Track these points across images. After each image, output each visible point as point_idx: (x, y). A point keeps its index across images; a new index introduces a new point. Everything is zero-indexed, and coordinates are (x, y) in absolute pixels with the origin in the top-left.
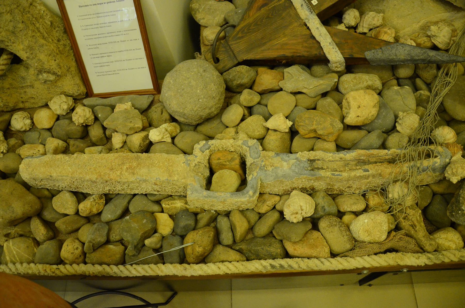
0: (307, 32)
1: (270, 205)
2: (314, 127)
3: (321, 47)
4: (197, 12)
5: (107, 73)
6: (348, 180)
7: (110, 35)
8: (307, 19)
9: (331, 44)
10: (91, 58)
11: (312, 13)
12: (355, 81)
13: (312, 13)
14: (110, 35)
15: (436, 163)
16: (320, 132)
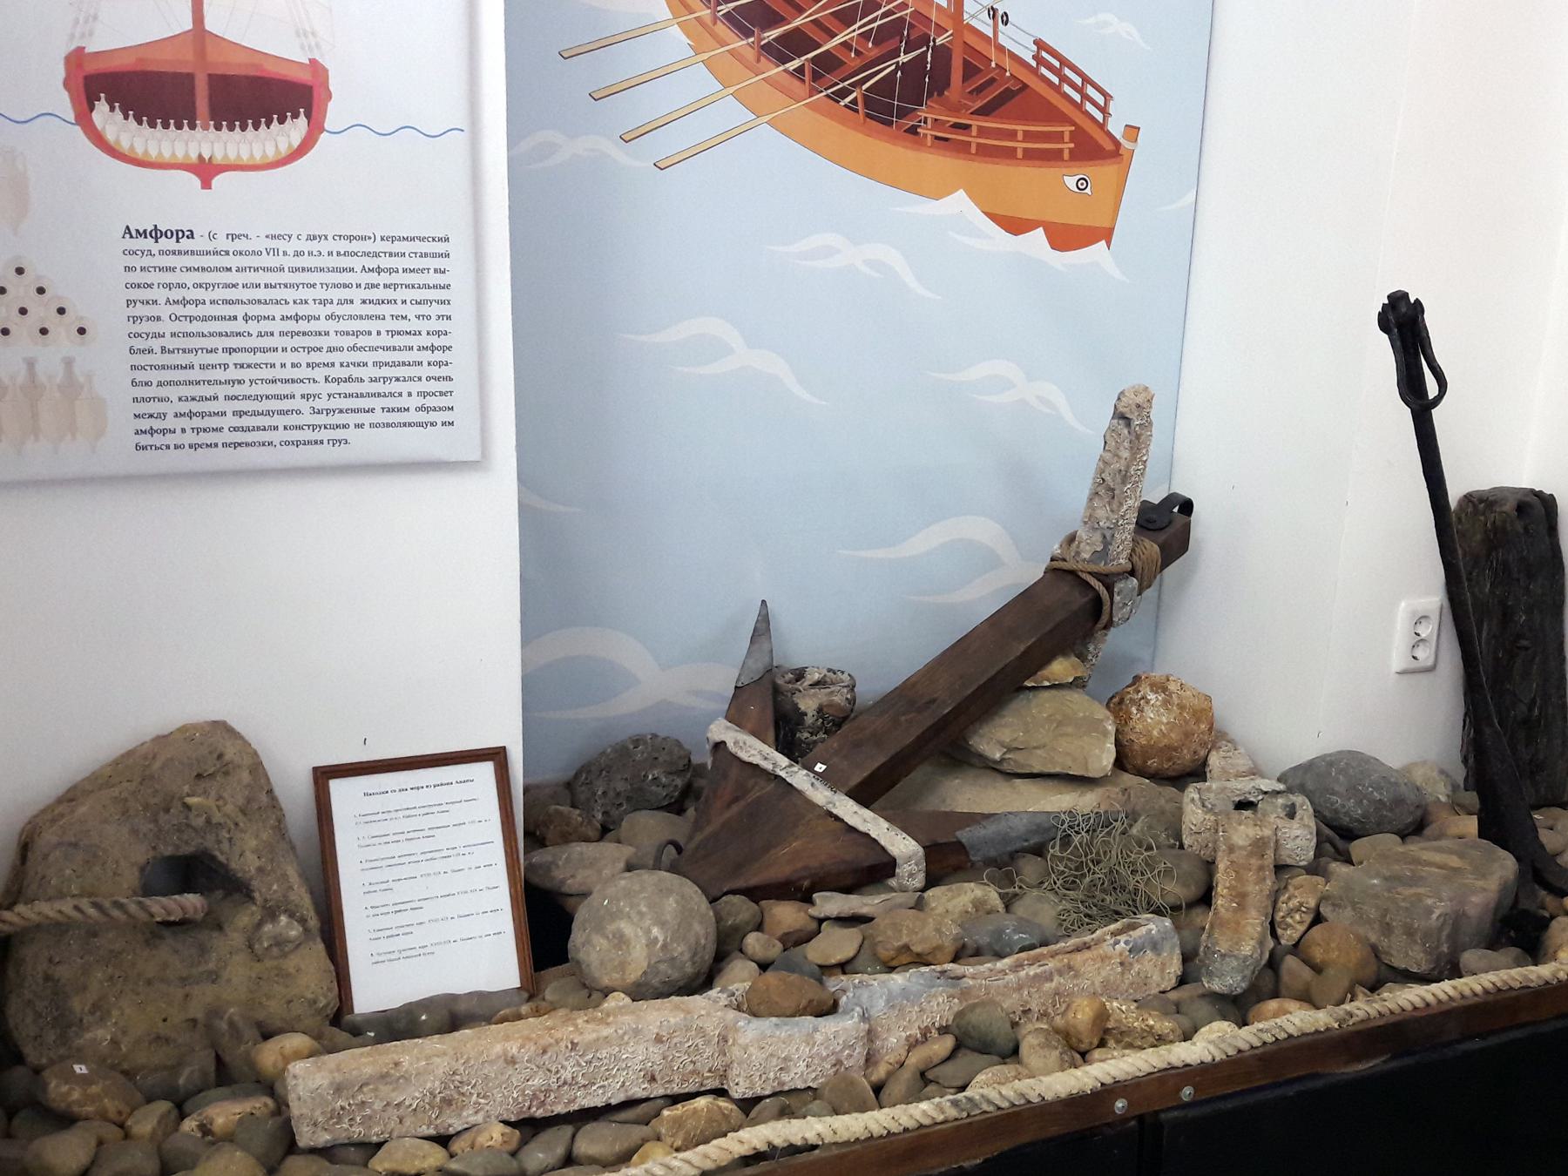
1: (891, 1061)
2: (905, 940)
3: (875, 840)
4: (553, 867)
5: (405, 954)
6: (1019, 988)
7: (429, 856)
8: (830, 803)
10: (368, 916)
11: (835, 792)
12: (950, 894)
13: (835, 792)
14: (429, 856)
15: (1151, 930)
16: (917, 948)
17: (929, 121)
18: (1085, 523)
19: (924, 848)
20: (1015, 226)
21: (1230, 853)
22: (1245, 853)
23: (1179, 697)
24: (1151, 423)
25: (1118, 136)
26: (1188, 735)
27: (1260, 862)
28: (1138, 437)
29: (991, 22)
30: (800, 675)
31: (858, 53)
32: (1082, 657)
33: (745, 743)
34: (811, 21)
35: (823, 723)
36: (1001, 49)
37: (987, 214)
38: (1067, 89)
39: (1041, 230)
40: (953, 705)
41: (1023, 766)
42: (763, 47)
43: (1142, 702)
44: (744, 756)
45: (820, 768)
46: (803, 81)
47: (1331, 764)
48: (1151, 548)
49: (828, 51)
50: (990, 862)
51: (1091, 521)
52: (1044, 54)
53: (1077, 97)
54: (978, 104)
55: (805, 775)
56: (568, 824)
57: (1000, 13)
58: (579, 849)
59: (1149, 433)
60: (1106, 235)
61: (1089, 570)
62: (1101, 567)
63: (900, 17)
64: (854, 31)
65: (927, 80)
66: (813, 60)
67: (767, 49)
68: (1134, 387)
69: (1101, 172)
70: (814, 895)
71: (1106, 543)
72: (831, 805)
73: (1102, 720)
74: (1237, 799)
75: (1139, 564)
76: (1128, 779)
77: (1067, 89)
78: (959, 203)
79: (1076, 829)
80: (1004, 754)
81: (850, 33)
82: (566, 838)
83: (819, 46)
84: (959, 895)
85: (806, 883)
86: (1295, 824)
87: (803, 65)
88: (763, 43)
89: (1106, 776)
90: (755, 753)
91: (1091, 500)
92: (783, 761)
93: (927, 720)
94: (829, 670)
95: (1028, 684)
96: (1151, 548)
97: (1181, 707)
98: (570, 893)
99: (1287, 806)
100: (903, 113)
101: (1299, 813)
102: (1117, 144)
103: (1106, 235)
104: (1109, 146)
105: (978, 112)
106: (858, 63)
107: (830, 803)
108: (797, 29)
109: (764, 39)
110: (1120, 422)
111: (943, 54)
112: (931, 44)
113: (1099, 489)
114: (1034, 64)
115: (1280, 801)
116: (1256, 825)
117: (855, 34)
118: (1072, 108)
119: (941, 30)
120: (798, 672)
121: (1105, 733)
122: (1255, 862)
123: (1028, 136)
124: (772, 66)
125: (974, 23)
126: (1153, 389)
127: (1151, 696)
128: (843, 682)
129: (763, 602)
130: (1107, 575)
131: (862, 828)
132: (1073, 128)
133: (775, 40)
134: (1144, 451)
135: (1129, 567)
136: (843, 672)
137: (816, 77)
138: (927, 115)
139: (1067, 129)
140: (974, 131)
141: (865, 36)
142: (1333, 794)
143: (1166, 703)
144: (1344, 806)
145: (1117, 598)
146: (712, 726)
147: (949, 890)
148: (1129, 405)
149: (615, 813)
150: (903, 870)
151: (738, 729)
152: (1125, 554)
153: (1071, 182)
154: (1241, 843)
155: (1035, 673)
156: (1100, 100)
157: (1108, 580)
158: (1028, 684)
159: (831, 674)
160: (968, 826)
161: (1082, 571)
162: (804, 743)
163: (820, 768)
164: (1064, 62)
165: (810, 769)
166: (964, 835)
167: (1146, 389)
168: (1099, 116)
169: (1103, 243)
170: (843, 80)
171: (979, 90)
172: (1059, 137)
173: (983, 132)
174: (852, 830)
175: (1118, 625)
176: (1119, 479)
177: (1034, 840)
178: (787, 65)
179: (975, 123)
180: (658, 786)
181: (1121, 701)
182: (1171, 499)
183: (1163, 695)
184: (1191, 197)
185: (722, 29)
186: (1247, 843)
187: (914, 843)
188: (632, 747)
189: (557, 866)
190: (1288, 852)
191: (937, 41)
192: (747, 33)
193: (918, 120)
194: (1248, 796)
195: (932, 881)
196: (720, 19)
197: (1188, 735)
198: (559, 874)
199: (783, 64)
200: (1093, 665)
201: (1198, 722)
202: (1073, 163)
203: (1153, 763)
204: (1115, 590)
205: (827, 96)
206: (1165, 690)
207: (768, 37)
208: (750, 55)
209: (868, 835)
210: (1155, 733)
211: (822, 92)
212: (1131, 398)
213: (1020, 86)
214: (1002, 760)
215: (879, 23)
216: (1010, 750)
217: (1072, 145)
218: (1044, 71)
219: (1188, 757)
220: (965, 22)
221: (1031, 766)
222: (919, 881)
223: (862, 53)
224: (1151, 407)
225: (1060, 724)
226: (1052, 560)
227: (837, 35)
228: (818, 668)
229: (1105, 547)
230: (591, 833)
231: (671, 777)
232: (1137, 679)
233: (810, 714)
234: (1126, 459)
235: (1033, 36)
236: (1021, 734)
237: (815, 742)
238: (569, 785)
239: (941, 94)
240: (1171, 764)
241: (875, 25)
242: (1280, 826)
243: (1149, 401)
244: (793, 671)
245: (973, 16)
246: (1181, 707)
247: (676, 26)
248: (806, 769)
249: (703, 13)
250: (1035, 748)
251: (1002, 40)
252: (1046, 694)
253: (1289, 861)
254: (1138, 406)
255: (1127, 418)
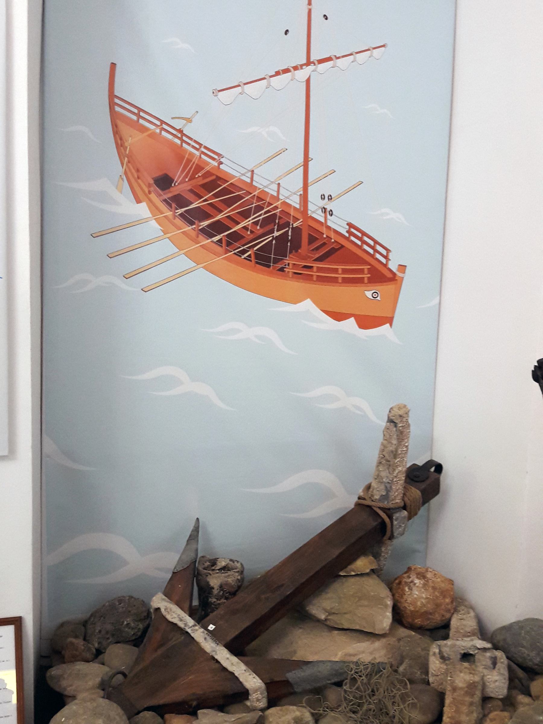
0: (217, 665)
9: (246, 671)
11: (218, 644)
12: (281, 713)
17: (290, 264)
18: (376, 479)
19: (265, 683)
20: (338, 316)
21: (453, 692)
22: (462, 692)
23: (433, 582)
24: (409, 426)
25: (394, 270)
26: (438, 605)
27: (471, 700)
28: (402, 433)
29: (323, 215)
30: (214, 562)
31: (252, 232)
32: (377, 556)
33: (171, 610)
34: (226, 217)
35: (223, 593)
36: (329, 228)
37: (322, 310)
38: (365, 247)
39: (352, 319)
40: (294, 588)
41: (337, 624)
42: (201, 230)
43: (411, 584)
44: (169, 617)
45: (211, 627)
46: (222, 246)
47: (522, 628)
48: (415, 493)
49: (235, 231)
50: (306, 692)
51: (378, 477)
52: (352, 230)
53: (371, 251)
54: (317, 256)
55: (201, 632)
56: (76, 650)
57: (328, 210)
58: (81, 666)
59: (408, 431)
60: (390, 320)
61: (378, 506)
62: (385, 504)
63: (274, 213)
64: (249, 221)
65: (289, 244)
66: (227, 236)
67: (203, 231)
68: (398, 405)
69: (387, 288)
70: (199, 711)
71: (388, 490)
72: (214, 653)
73: (383, 598)
74: (463, 652)
75: (408, 502)
76: (403, 632)
77: (365, 247)
78: (308, 305)
79: (360, 674)
80: (327, 616)
81: (246, 223)
82: (75, 659)
83: (231, 229)
84: (287, 714)
85: (194, 703)
86: (495, 673)
87: (221, 238)
88: (200, 228)
89: (385, 634)
90: (175, 616)
91: (378, 466)
92: (191, 622)
93: (277, 597)
94: (231, 560)
95: (342, 573)
96: (415, 493)
97: (434, 588)
98: (70, 695)
99: (492, 657)
100: (276, 261)
101: (499, 665)
102: (394, 274)
103: (390, 320)
104: (389, 275)
105: (316, 260)
106: (252, 236)
107: (214, 651)
108: (218, 221)
109: (201, 226)
110: (392, 424)
111: (297, 231)
112: (291, 226)
113: (382, 460)
114: (347, 235)
115: (488, 654)
116: (471, 673)
117: (250, 222)
118: (369, 257)
119: (296, 219)
120: (212, 561)
121: (386, 606)
122: (468, 699)
123: (345, 271)
124: (205, 239)
125: (314, 215)
126: (409, 407)
127: (417, 581)
128: (236, 569)
129: (198, 519)
130: (389, 509)
131: (230, 669)
132: (369, 267)
133: (207, 226)
134: (406, 440)
135: (402, 504)
136: (238, 562)
137: (229, 244)
138: (289, 262)
139: (366, 267)
140: (315, 269)
141: (256, 223)
142: (522, 647)
143: (425, 585)
144: (528, 655)
145: (395, 523)
146: (154, 598)
147: (281, 710)
148: (395, 415)
149: (105, 643)
150: (253, 696)
151: (169, 600)
152: (399, 497)
153: (369, 294)
154: (461, 685)
155: (346, 567)
156: (384, 252)
157: (390, 512)
158: (342, 573)
159: (231, 563)
160: (294, 670)
161: (374, 506)
162: (214, 605)
163: (211, 627)
164: (364, 234)
165: (206, 628)
166: (291, 676)
167: (405, 406)
168: (384, 260)
169: (388, 325)
170: (243, 246)
171: (317, 249)
172: (361, 271)
173: (319, 269)
174: (225, 669)
175: (397, 537)
176: (392, 456)
177: (336, 680)
178: (213, 239)
179: (316, 265)
180: (129, 628)
181: (400, 583)
182: (430, 463)
183: (424, 581)
184: (437, 301)
185: (179, 222)
186: (464, 685)
187: (260, 681)
188: (118, 604)
189: (64, 678)
190: (491, 690)
191: (294, 225)
192: (192, 223)
193: (285, 264)
194: (469, 650)
195: (272, 702)
196: (177, 217)
197: (438, 605)
198: (64, 683)
199: (211, 238)
200: (386, 558)
201: (444, 597)
202: (369, 284)
203: (418, 621)
204: (394, 518)
205: (235, 253)
206: (424, 577)
207: (203, 225)
208: (193, 234)
209: (233, 674)
210: (419, 604)
211: (231, 251)
212: (396, 412)
213: (340, 246)
214: (326, 620)
215: (263, 217)
216: (330, 614)
217: (369, 275)
218: (353, 238)
219: (439, 619)
220: (309, 215)
221: (342, 624)
222: (263, 704)
223: (254, 232)
224: (408, 417)
225: (360, 599)
226: (359, 498)
227: (240, 223)
228: (224, 558)
229: (387, 494)
230: (88, 655)
231: (137, 623)
232: (409, 569)
233: (216, 589)
234: (395, 445)
235: (345, 221)
236: (337, 605)
237: (219, 604)
238: (85, 623)
239: (297, 251)
240: (428, 622)
241: (261, 218)
242: (485, 674)
243: (406, 413)
244: (210, 561)
245: (314, 212)
246: (434, 588)
247: (154, 220)
248: (204, 629)
249: (168, 214)
250: (345, 613)
251: (329, 224)
252: (352, 580)
253: (492, 695)
254: (401, 416)
255: (395, 422)
